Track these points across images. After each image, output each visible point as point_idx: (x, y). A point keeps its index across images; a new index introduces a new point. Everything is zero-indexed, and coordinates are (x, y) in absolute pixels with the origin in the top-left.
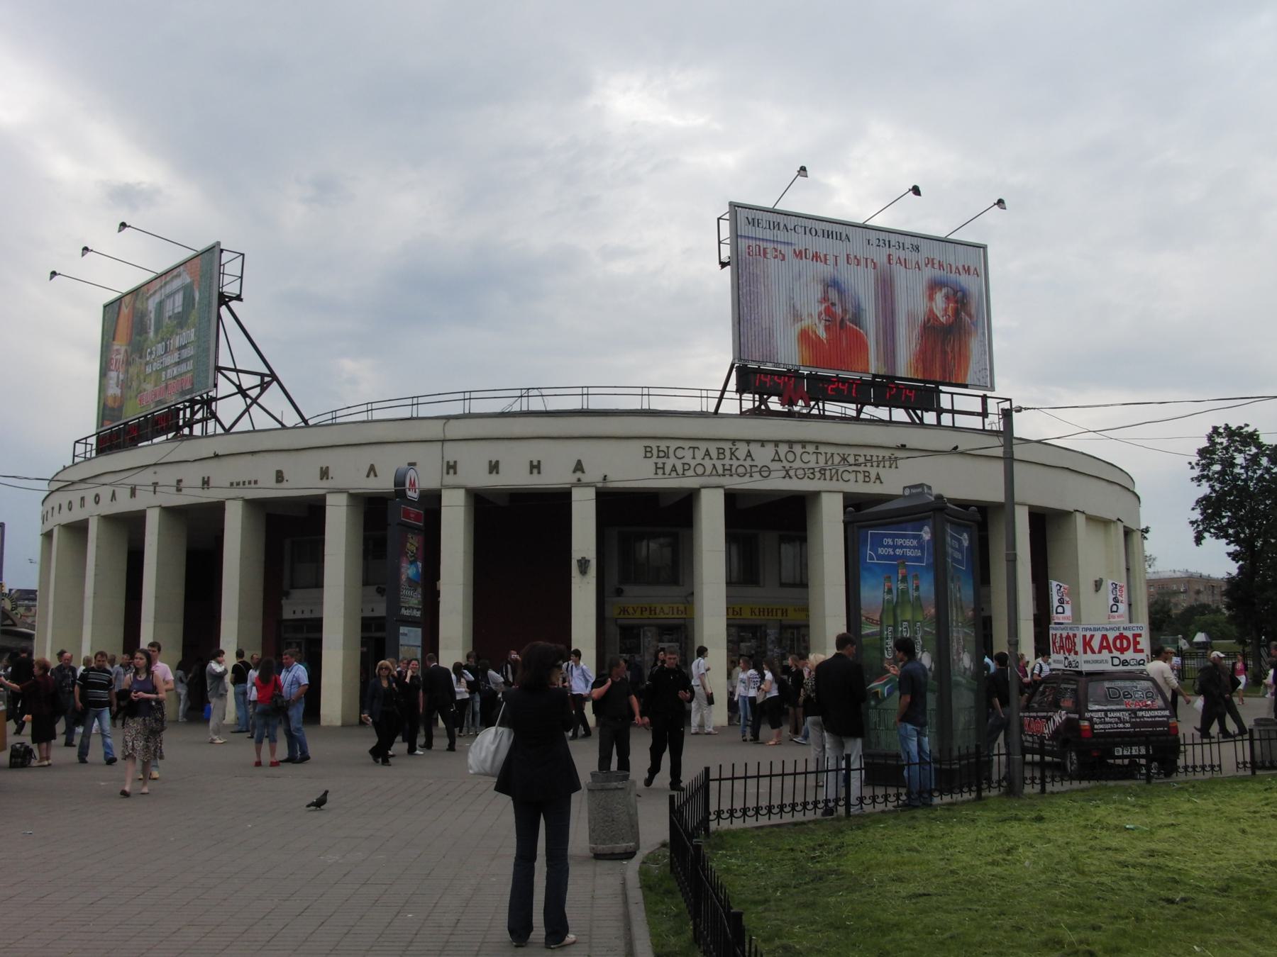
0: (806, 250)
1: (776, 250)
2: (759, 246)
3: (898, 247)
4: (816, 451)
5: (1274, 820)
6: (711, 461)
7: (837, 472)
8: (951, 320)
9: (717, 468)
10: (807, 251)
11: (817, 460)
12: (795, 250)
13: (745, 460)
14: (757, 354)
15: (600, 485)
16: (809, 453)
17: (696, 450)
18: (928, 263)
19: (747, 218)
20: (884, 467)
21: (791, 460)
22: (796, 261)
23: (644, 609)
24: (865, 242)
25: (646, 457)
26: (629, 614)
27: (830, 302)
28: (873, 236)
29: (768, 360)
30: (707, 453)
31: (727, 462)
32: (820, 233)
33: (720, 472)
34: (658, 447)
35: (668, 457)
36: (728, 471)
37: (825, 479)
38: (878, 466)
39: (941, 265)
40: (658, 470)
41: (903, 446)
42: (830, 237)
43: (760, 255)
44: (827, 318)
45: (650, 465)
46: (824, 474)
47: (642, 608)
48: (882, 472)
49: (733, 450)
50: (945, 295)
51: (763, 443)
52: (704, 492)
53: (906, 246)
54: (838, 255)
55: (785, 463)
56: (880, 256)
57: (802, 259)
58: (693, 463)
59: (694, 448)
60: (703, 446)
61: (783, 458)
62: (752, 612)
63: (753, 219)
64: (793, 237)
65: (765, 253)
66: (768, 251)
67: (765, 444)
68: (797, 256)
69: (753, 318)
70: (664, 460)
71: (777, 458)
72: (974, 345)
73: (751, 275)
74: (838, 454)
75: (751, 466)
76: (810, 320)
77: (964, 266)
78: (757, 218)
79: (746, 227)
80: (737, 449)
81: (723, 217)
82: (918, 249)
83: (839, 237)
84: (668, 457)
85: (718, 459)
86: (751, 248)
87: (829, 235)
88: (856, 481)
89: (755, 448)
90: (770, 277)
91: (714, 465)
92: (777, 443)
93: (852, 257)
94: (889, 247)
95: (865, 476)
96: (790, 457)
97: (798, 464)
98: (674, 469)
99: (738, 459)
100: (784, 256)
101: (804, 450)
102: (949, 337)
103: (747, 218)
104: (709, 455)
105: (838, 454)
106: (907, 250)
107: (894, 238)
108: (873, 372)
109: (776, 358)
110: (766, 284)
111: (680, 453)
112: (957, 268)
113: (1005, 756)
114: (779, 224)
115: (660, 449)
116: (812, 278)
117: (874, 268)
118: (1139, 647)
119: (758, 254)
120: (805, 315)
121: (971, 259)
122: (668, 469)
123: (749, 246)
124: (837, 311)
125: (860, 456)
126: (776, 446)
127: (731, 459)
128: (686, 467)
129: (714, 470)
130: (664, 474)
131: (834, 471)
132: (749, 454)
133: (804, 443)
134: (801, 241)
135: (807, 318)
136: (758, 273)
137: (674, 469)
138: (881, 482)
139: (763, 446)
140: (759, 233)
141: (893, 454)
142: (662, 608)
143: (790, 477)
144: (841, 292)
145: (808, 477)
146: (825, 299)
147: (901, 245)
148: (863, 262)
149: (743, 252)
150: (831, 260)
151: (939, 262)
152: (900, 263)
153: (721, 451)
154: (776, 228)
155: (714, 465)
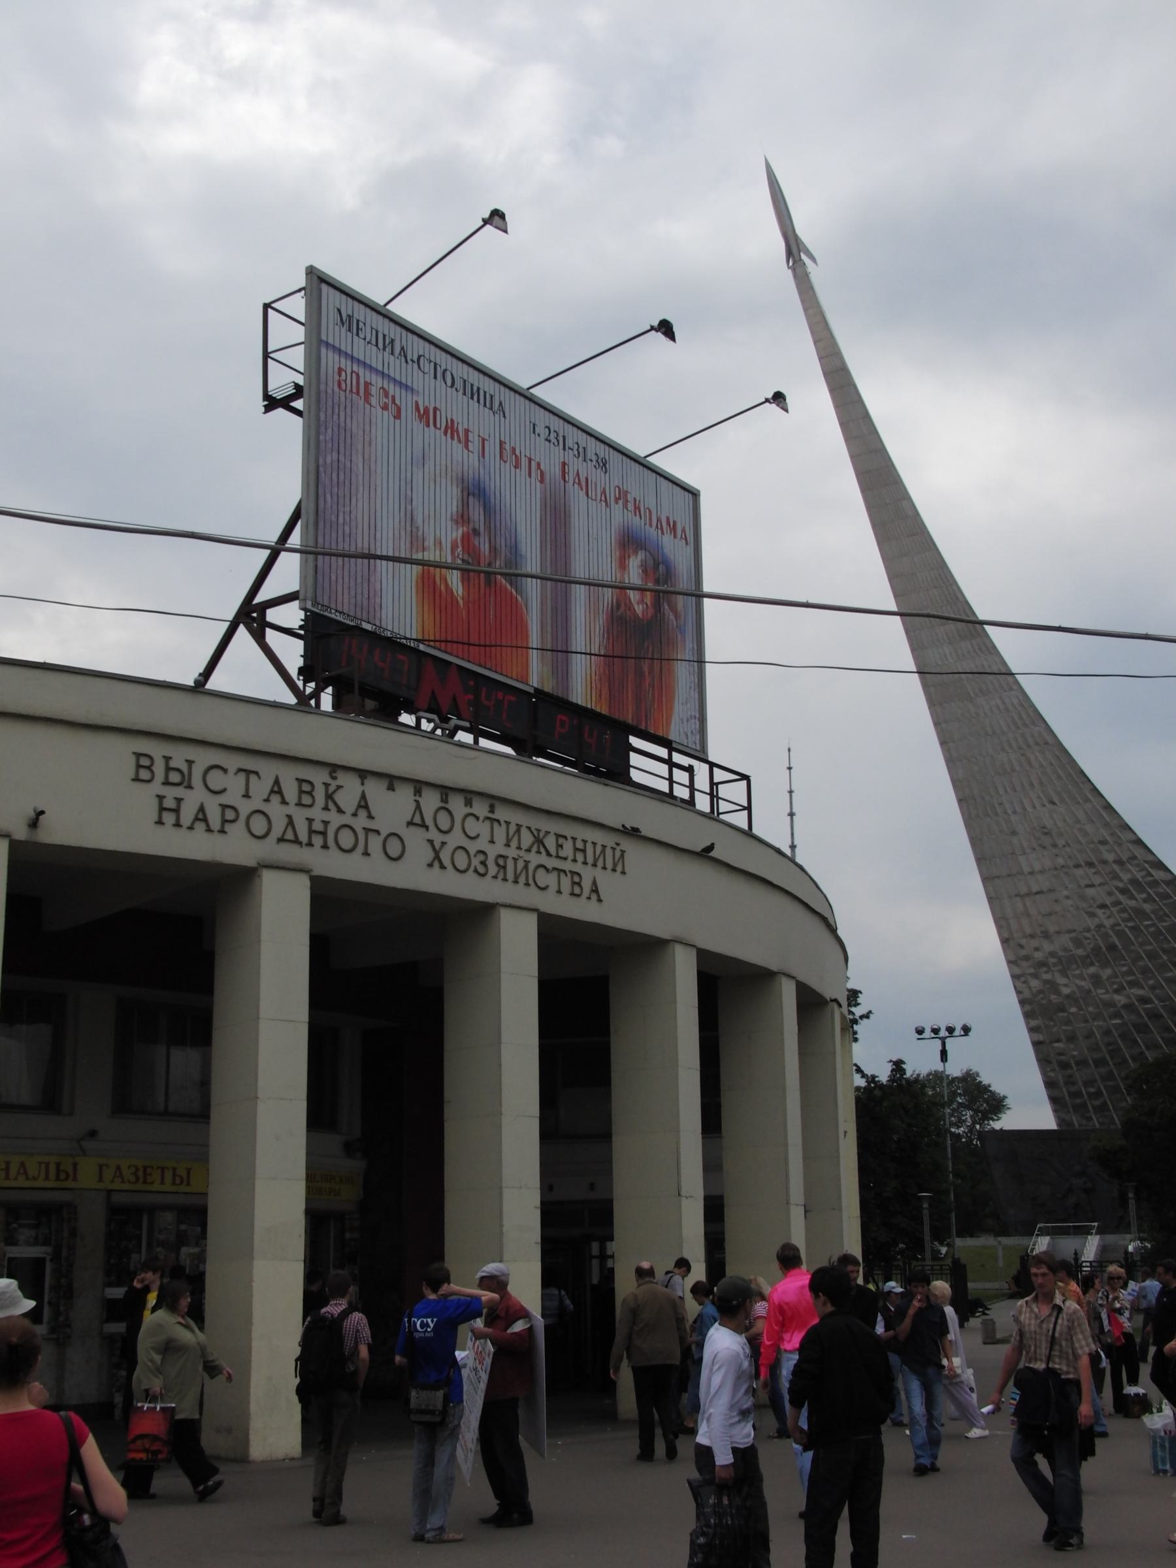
0: (435, 409)
1: (386, 394)
2: (358, 375)
3: (576, 453)
4: (490, 815)
5: (687, 1485)
6: (284, 807)
7: (526, 867)
8: (649, 615)
10: (438, 412)
11: (492, 836)
12: (417, 403)
13: (355, 815)
14: (346, 601)
15: (21, 833)
17: (253, 778)
18: (619, 498)
19: (339, 311)
21: (445, 827)
22: (418, 426)
24: (529, 427)
25: (137, 779)
27: (471, 526)
28: (542, 418)
29: (365, 617)
30: (277, 789)
31: (317, 813)
32: (459, 384)
33: (303, 836)
34: (167, 759)
35: (190, 787)
36: (319, 834)
37: (505, 880)
39: (637, 508)
40: (165, 815)
41: (635, 830)
42: (475, 397)
43: (358, 393)
44: (466, 557)
45: (145, 798)
46: (504, 868)
49: (331, 789)
50: (642, 566)
51: (392, 781)
52: (267, 876)
53: (589, 456)
54: (487, 437)
55: (433, 834)
56: (550, 458)
57: (428, 426)
58: (245, 807)
59: (248, 772)
60: (269, 770)
61: (429, 821)
63: (349, 316)
64: (416, 378)
65: (368, 394)
66: (373, 390)
67: (396, 784)
68: (421, 417)
69: (341, 520)
70: (179, 792)
71: (417, 820)
72: (682, 672)
73: (342, 432)
74: (529, 828)
75: (367, 830)
76: (438, 552)
77: (668, 519)
78: (356, 316)
79: (337, 328)
81: (273, 305)
82: (604, 465)
83: (488, 402)
84: (190, 787)
85: (299, 804)
86: (343, 374)
87: (474, 393)
88: (559, 892)
89: (375, 791)
90: (373, 444)
91: (289, 817)
92: (419, 786)
93: (507, 447)
94: (564, 449)
96: (444, 822)
97: (456, 839)
98: (201, 816)
99: (340, 811)
100: (399, 409)
102: (646, 645)
103: (339, 311)
104: (280, 792)
105: (529, 828)
106: (589, 462)
107: (573, 435)
108: (535, 685)
109: (378, 615)
110: (366, 456)
112: (659, 520)
114: (392, 341)
115: (172, 764)
116: (444, 468)
117: (542, 481)
118: (133, 1169)
119: (354, 391)
120: (429, 542)
121: (672, 506)
122: (188, 813)
123: (340, 370)
124: (482, 549)
126: (418, 792)
127: (326, 808)
128: (230, 815)
129: (290, 828)
130: (178, 825)
131: (521, 864)
132: (363, 804)
133: (469, 795)
134: (431, 392)
135: (432, 547)
136: (354, 430)
137: (201, 816)
138: (600, 900)
139: (391, 788)
140: (359, 349)
141: (618, 844)
142: (22, 1164)
143: (442, 867)
144: (489, 510)
145: (476, 871)
146: (462, 518)
147: (581, 450)
148: (524, 462)
149: (330, 378)
150: (475, 445)
151: (635, 499)
152: (579, 484)
153: (306, 787)
154: (388, 349)
155: (289, 817)
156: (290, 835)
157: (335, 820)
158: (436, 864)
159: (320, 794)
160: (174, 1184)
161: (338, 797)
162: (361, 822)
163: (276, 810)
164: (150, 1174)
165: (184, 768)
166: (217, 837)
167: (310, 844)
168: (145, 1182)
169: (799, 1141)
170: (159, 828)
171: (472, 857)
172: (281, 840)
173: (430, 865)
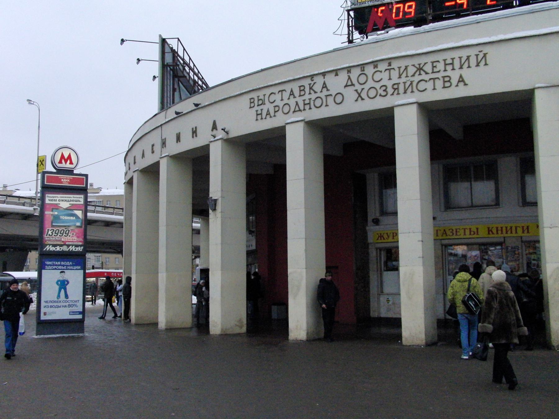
4: (389, 67)
9: (300, 105)
16: (381, 72)
20: (469, 67)
23: (395, 234)
26: (384, 239)
30: (292, 93)
31: (307, 97)
33: (302, 108)
37: (398, 94)
38: (461, 68)
46: (398, 89)
47: (393, 233)
48: (465, 73)
49: (311, 85)
52: (288, 128)
58: (281, 104)
59: (282, 91)
60: (288, 87)
62: (490, 231)
80: (314, 83)
88: (434, 89)
89: (330, 80)
91: (297, 102)
92: (349, 69)
95: (444, 82)
98: (268, 113)
101: (376, 69)
104: (293, 94)
111: (272, 98)
113: (62, 262)
118: (451, 231)
125: (438, 61)
129: (297, 106)
130: (271, 117)
132: (325, 86)
137: (268, 113)
138: (466, 84)
143: (362, 99)
145: (380, 95)
155: (297, 102)
156: (297, 109)
157: (313, 96)
158: (360, 99)
159: (307, 90)
160: (470, 234)
161: (314, 88)
162: (322, 95)
163: (292, 102)
164: (459, 232)
165: (263, 98)
166: (274, 118)
167: (304, 110)
168: (456, 235)
169: (133, 225)
170: (271, 118)
171: (334, 96)
172: (294, 112)
173: (357, 100)
